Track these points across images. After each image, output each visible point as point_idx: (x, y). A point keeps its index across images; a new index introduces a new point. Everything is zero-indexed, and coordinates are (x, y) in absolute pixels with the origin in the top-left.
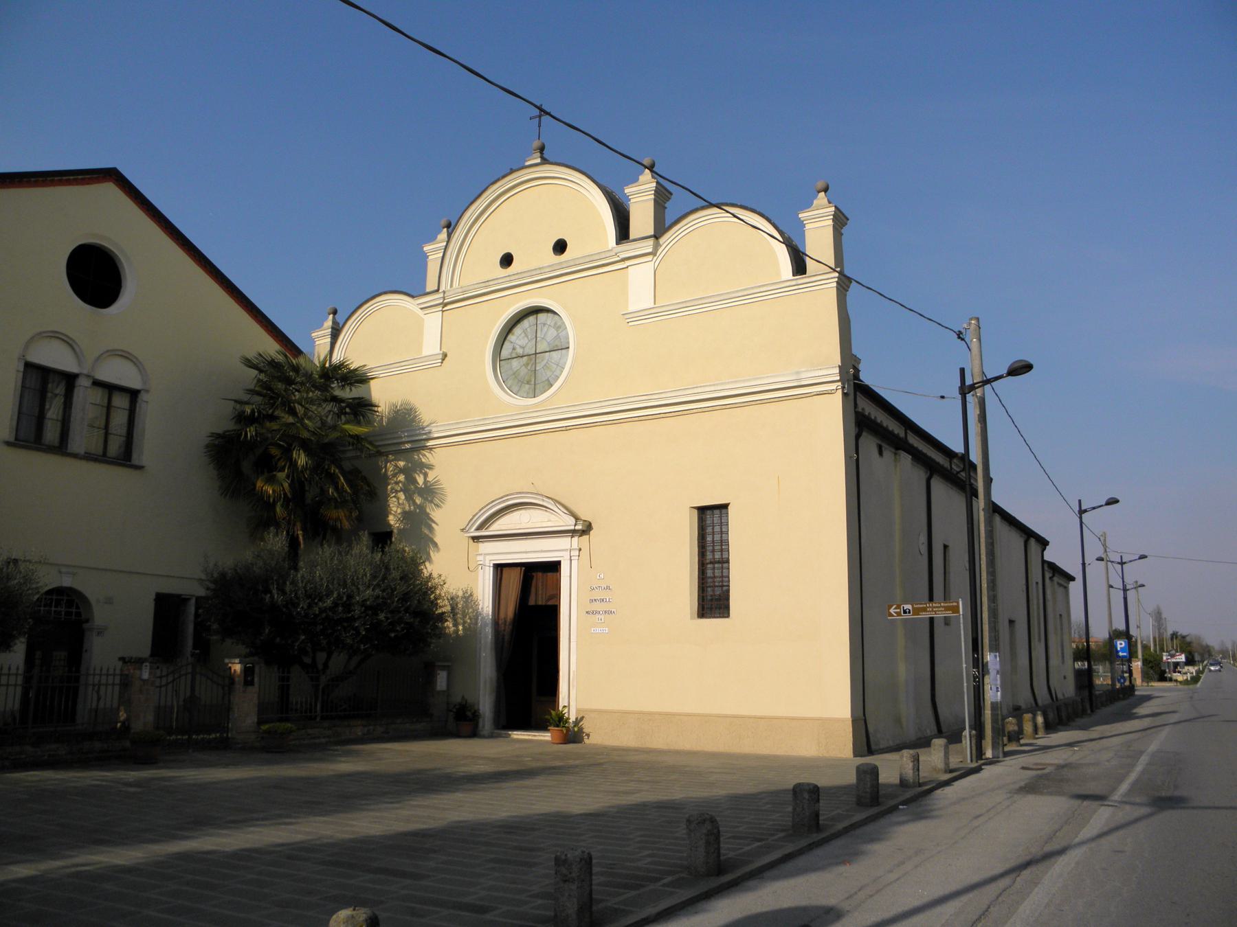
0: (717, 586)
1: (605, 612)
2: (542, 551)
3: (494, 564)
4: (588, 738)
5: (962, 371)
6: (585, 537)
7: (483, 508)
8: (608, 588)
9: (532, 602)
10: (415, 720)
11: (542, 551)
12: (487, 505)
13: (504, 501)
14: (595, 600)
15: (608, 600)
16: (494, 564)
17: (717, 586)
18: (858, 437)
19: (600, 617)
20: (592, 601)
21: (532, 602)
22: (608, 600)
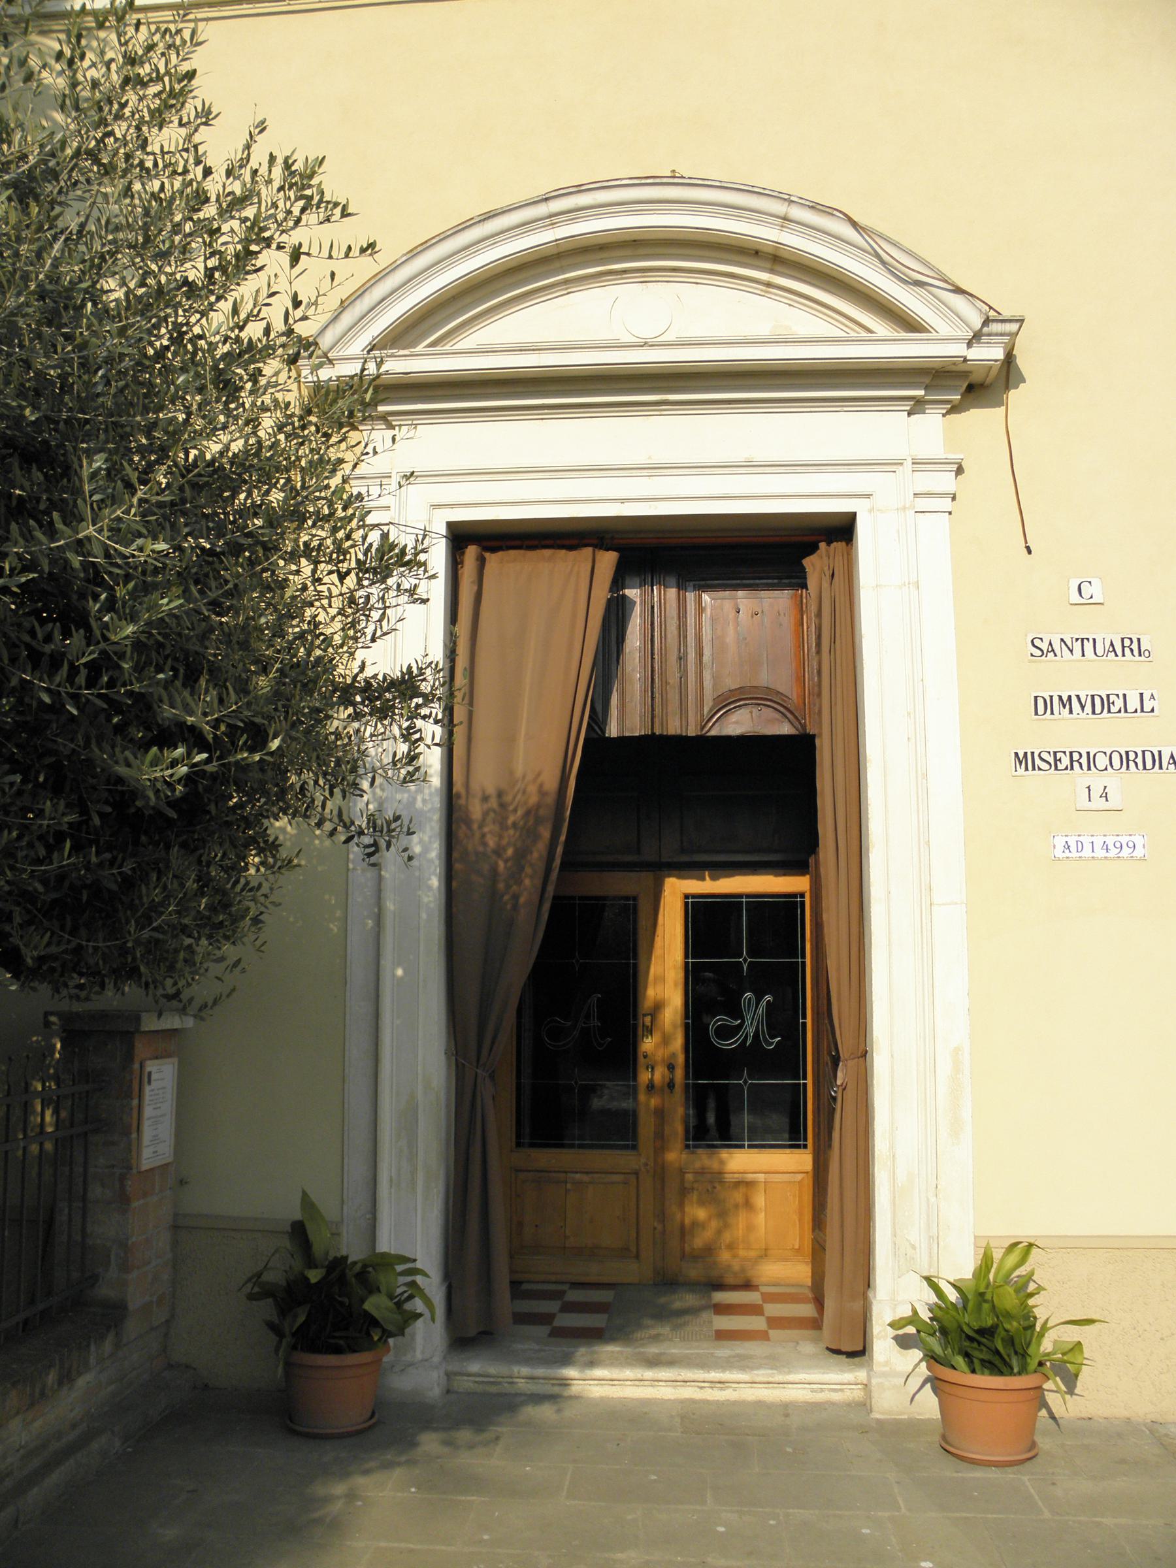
0: (128, 130)
1: (1126, 759)
2: (750, 466)
3: (450, 525)
4: (1071, 1390)
5: (1107, 800)
6: (980, 419)
7: (426, 246)
8: (1131, 646)
9: (613, 731)
10: (51, 1377)
11: (750, 466)
12: (443, 237)
13: (552, 219)
14: (1066, 703)
15: (1133, 703)
16: (450, 525)
17: (128, 130)
18: (308, 1436)
19: (1097, 781)
20: (1044, 706)
21: (613, 731)
22: (1133, 703)
